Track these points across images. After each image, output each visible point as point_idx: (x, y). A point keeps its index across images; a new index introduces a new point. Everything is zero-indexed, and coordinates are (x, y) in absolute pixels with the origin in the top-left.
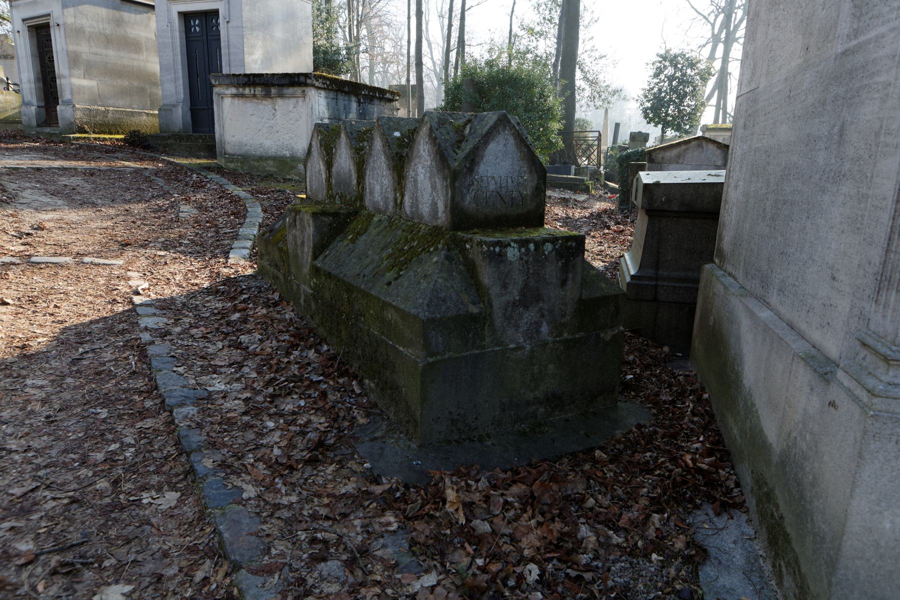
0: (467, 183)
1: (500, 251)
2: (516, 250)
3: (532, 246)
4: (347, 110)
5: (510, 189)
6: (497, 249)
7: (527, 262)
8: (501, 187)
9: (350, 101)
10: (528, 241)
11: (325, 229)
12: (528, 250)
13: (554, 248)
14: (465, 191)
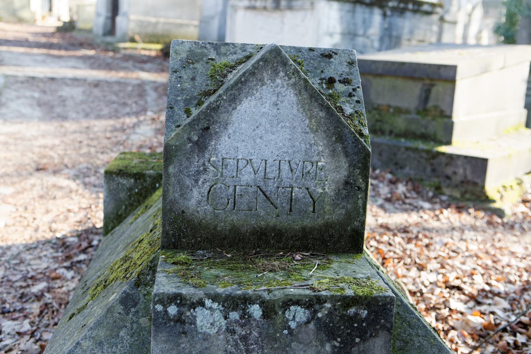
0: (193, 169)
1: (180, 313)
2: (218, 315)
3: (256, 311)
4: (367, 24)
5: (286, 182)
6: (173, 310)
7: (244, 338)
8: (265, 178)
9: (371, 13)
10: (247, 300)
11: (122, 195)
12: (246, 316)
13: (313, 317)
14: (188, 182)
